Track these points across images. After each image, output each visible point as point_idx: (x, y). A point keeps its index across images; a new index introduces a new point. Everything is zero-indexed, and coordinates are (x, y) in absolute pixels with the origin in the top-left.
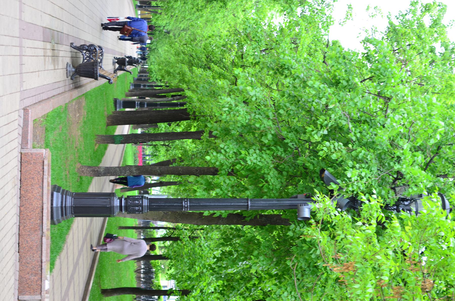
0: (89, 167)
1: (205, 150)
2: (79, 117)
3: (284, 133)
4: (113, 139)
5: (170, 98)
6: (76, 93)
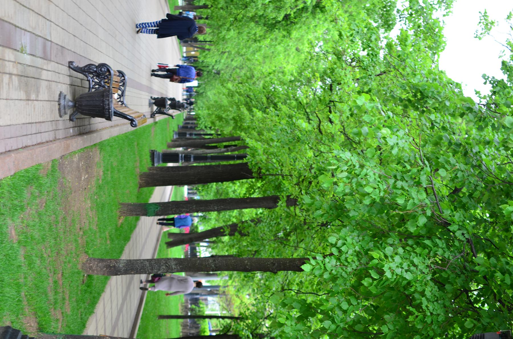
0: (102, 260)
1: (275, 222)
2: (88, 180)
3: (447, 213)
4: (143, 209)
5: (223, 149)
6: (78, 144)
